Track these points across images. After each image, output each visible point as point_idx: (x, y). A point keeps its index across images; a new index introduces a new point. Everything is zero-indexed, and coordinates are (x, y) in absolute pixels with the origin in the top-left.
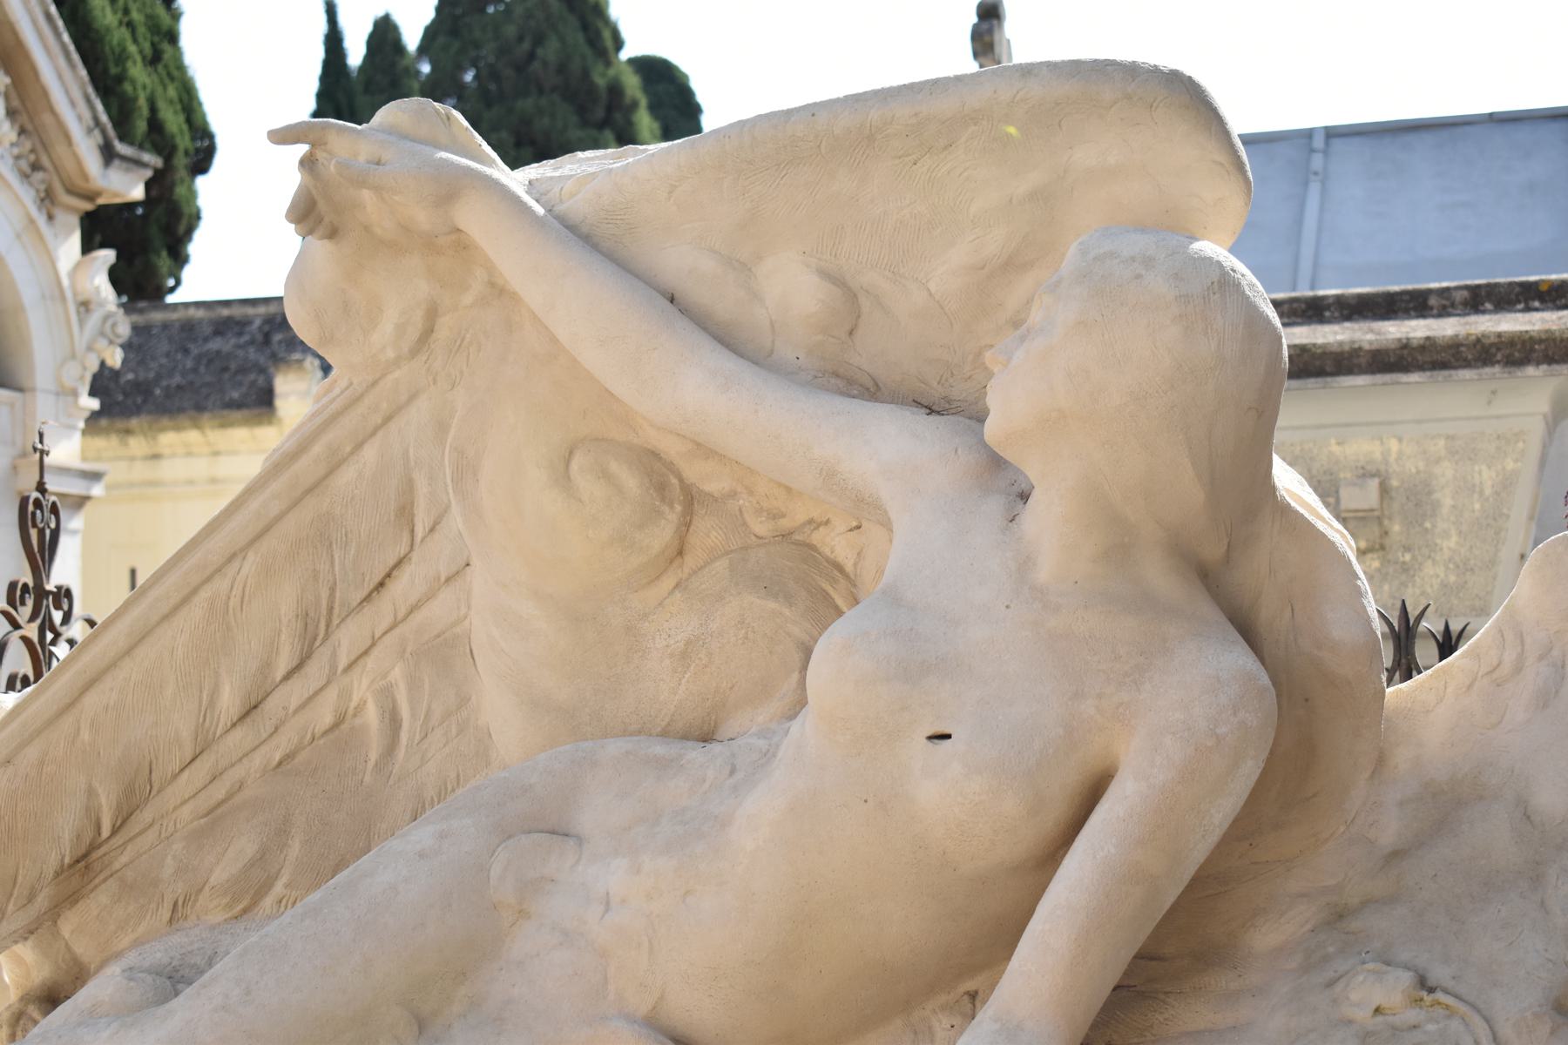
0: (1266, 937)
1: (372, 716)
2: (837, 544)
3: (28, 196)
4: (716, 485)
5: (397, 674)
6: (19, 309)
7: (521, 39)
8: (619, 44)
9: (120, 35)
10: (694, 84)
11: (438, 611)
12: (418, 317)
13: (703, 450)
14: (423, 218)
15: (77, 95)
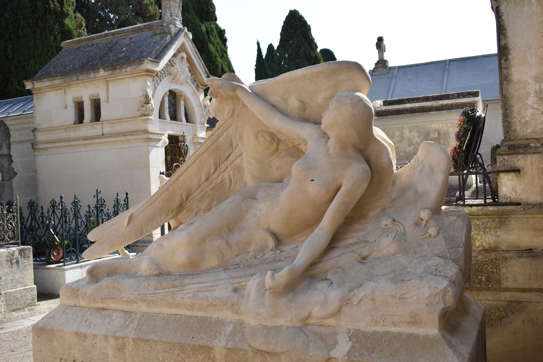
0: (372, 214)
1: (227, 180)
2: (302, 148)
3: (194, 86)
4: (283, 138)
5: (231, 173)
7: (296, 47)
8: (317, 47)
9: (215, 53)
10: (335, 54)
11: (238, 162)
12: (231, 110)
13: (280, 132)
15: (202, 67)
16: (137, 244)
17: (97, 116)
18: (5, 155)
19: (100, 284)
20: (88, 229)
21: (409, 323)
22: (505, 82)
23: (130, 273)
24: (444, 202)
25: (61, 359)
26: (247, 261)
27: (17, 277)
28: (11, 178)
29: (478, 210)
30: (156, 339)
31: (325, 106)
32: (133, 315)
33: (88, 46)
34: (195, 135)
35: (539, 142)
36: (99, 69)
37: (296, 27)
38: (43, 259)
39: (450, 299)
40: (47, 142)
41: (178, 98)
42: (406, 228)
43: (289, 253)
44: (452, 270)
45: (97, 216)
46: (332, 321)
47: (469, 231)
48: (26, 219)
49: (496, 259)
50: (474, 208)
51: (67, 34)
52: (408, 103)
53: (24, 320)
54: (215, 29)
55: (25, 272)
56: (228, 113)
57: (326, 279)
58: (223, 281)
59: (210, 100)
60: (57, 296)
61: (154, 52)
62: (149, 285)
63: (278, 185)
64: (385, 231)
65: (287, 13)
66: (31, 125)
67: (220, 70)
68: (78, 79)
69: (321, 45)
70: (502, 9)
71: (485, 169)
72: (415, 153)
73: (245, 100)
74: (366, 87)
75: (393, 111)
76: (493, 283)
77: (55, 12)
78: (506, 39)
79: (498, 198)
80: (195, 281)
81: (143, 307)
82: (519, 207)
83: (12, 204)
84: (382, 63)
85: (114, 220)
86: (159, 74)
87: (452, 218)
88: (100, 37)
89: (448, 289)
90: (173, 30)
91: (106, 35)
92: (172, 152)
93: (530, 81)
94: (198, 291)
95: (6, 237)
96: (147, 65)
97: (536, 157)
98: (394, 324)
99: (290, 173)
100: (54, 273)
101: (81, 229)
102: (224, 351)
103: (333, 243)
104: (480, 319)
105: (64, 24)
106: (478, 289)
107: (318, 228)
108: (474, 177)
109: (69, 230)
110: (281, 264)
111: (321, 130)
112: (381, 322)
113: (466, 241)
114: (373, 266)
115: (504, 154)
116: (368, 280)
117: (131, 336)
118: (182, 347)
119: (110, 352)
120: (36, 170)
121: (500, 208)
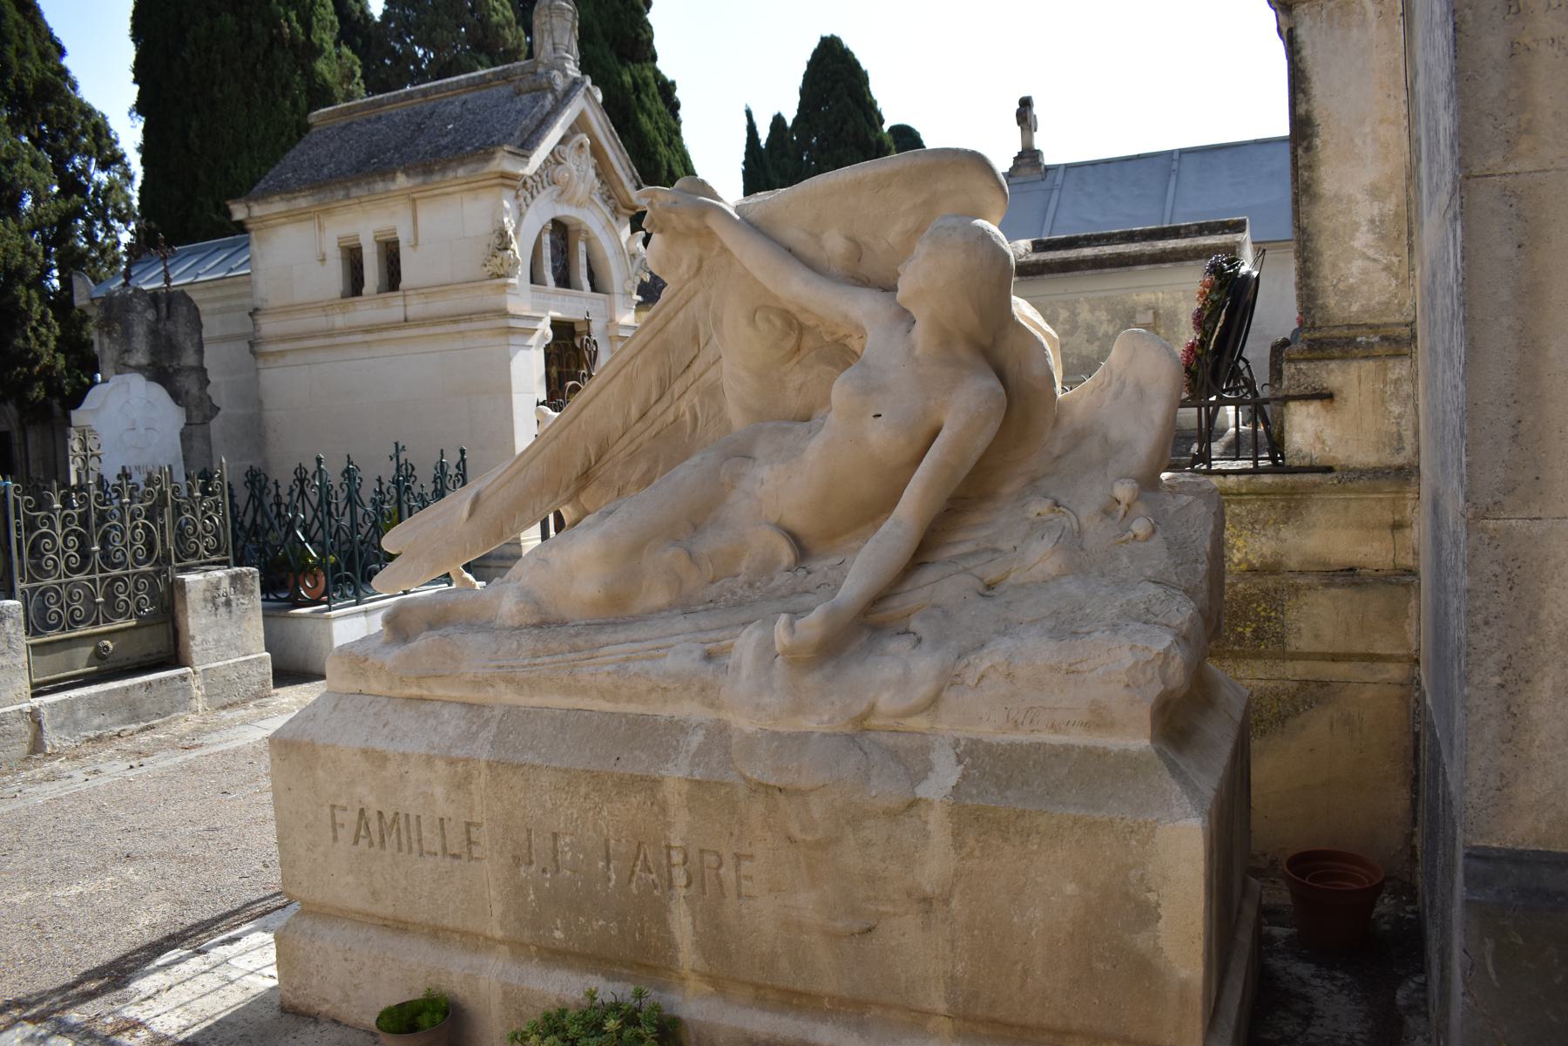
0: (1008, 489)
1: (688, 416)
2: (854, 344)
3: (607, 210)
4: (811, 323)
5: (696, 400)
6: (606, 259)
8: (882, 121)
9: (654, 134)
11: (711, 375)
13: (805, 310)
14: (694, 223)
16: (487, 563)
17: (392, 278)
18: (192, 369)
19: (413, 645)
20: (379, 530)
21: (1087, 726)
22: (1304, 200)
23: (479, 622)
24: (1166, 463)
25: (333, 807)
26: (733, 593)
27: (228, 635)
28: (207, 419)
29: (1239, 484)
30: (538, 762)
31: (906, 251)
32: (487, 711)
33: (369, 121)
34: (612, 320)
35: (1376, 334)
36: (394, 172)
37: (834, 75)
38: (283, 596)
39: (1177, 672)
40: (283, 339)
41: (571, 236)
42: (1083, 520)
43: (826, 575)
44: (1183, 612)
45: (399, 502)
46: (919, 723)
47: (1220, 528)
48: (242, 510)
49: (1276, 591)
50: (1232, 479)
51: (321, 95)
52: (1089, 245)
53: (246, 728)
54: (652, 81)
55: (245, 625)
56: (689, 267)
57: (907, 632)
58: (681, 638)
59: (646, 242)
60: (322, 677)
61: (517, 133)
62: (520, 646)
63: (801, 428)
64: (1037, 527)
65: (815, 44)
66: (247, 301)
67: (665, 174)
68: (347, 197)
69: (892, 115)
70: (1302, 33)
71: (1256, 394)
72: (1104, 354)
73: (729, 238)
74: (998, 207)
75: (1053, 264)
76: (1268, 641)
77: (293, 44)
78: (1308, 101)
79: (1283, 457)
80: (621, 636)
81: (507, 696)
82: (1330, 476)
83: (212, 477)
84: (1028, 157)
85: (435, 508)
86: (530, 182)
87: (1184, 499)
88: (396, 99)
89: (1173, 652)
90: (560, 83)
91: (409, 95)
92: (559, 357)
93: (1359, 197)
94: (628, 659)
95: (202, 549)
96: (503, 162)
97: (1370, 365)
98: (1054, 728)
99: (827, 400)
100: (307, 626)
101: (364, 531)
102: (686, 787)
103: (921, 554)
104: (1238, 717)
105: (313, 71)
106: (1236, 656)
107: (890, 521)
108: (1231, 410)
109: (337, 531)
110: (808, 599)
111: (898, 304)
112: (1027, 722)
113: (1212, 547)
114: (1009, 603)
115: (1300, 360)
116: (999, 633)
117: (484, 757)
118: (596, 778)
119: (439, 791)
120: (261, 402)
121: (1288, 477)
